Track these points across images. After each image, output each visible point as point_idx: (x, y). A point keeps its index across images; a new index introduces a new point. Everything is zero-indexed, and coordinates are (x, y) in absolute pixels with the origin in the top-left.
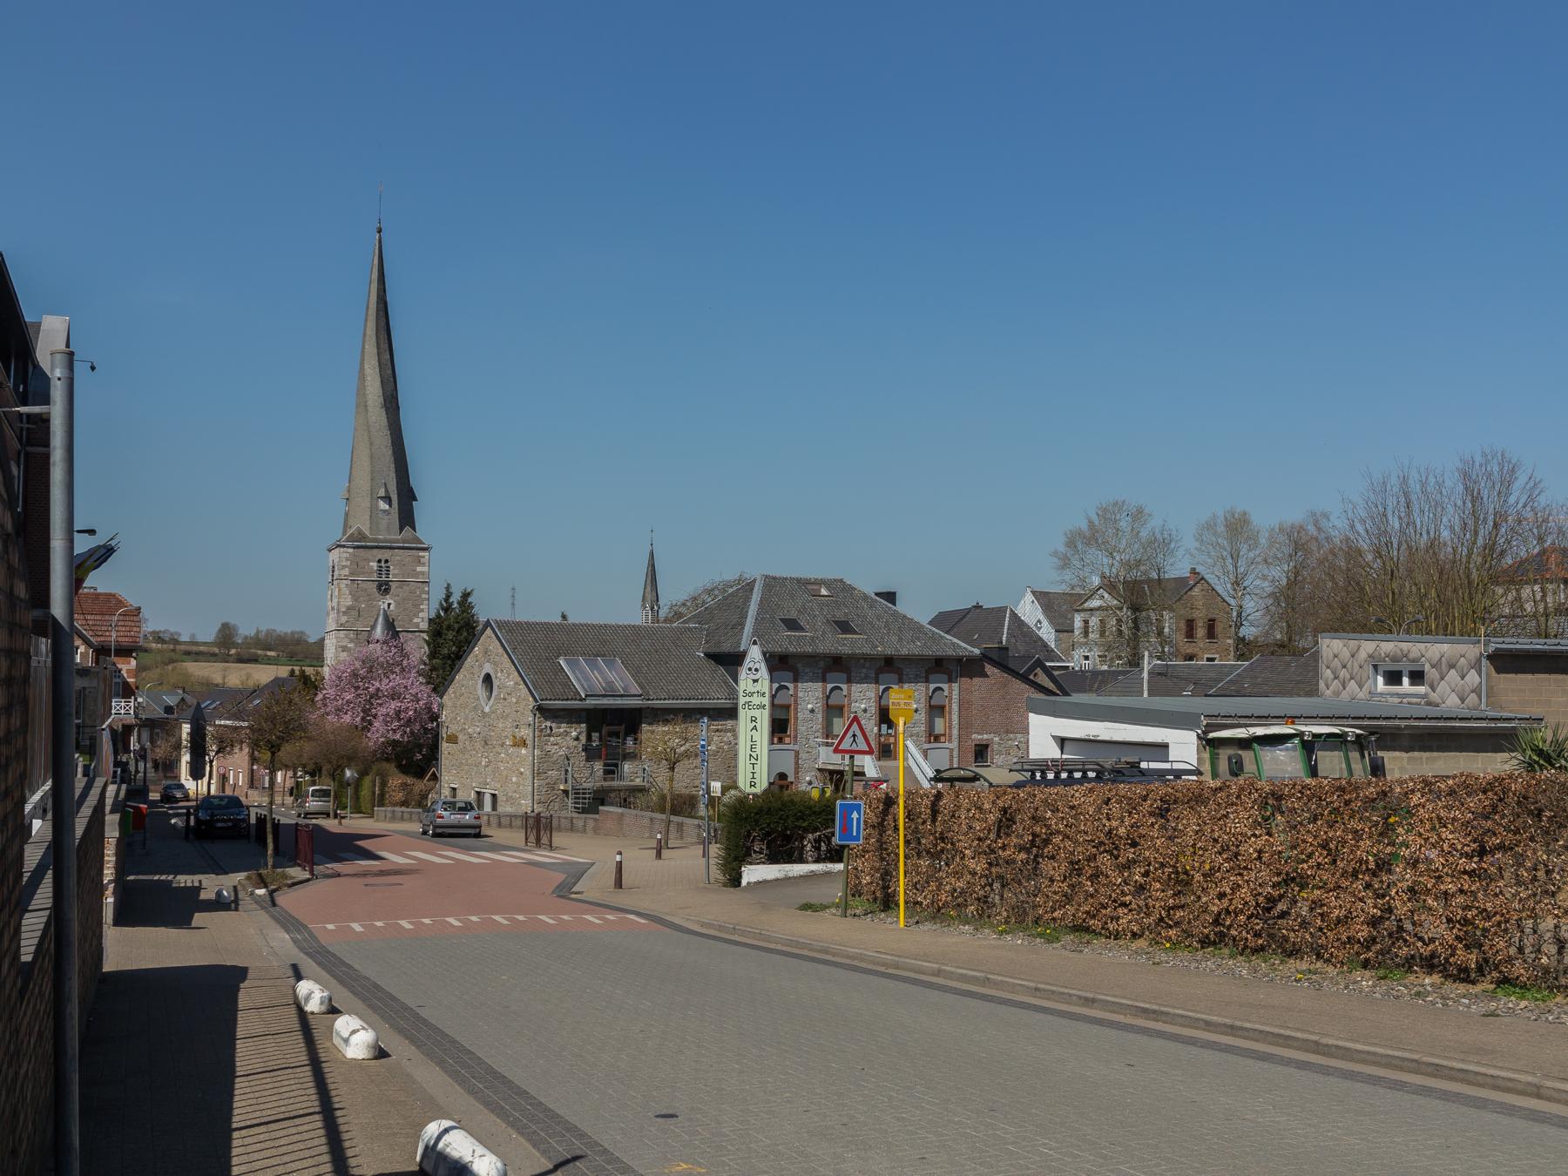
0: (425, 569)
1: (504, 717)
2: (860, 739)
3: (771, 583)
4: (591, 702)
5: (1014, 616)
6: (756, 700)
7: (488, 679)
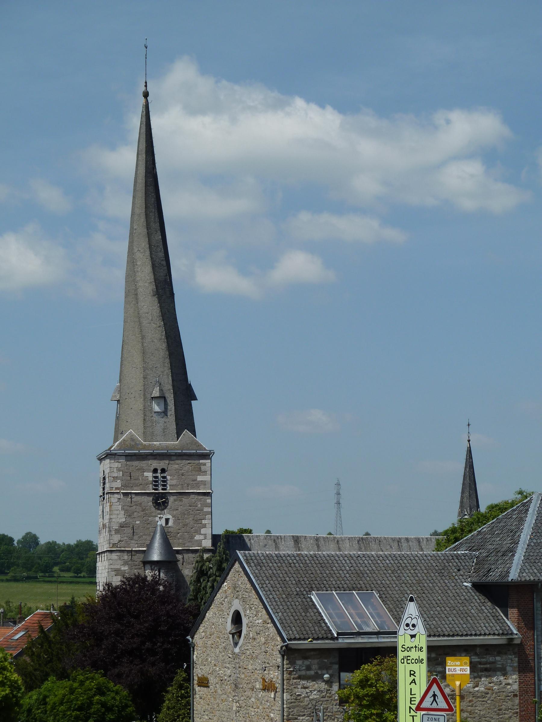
0: (207, 478)
2: (440, 699)
4: (344, 642)
6: (414, 654)
7: (237, 619)
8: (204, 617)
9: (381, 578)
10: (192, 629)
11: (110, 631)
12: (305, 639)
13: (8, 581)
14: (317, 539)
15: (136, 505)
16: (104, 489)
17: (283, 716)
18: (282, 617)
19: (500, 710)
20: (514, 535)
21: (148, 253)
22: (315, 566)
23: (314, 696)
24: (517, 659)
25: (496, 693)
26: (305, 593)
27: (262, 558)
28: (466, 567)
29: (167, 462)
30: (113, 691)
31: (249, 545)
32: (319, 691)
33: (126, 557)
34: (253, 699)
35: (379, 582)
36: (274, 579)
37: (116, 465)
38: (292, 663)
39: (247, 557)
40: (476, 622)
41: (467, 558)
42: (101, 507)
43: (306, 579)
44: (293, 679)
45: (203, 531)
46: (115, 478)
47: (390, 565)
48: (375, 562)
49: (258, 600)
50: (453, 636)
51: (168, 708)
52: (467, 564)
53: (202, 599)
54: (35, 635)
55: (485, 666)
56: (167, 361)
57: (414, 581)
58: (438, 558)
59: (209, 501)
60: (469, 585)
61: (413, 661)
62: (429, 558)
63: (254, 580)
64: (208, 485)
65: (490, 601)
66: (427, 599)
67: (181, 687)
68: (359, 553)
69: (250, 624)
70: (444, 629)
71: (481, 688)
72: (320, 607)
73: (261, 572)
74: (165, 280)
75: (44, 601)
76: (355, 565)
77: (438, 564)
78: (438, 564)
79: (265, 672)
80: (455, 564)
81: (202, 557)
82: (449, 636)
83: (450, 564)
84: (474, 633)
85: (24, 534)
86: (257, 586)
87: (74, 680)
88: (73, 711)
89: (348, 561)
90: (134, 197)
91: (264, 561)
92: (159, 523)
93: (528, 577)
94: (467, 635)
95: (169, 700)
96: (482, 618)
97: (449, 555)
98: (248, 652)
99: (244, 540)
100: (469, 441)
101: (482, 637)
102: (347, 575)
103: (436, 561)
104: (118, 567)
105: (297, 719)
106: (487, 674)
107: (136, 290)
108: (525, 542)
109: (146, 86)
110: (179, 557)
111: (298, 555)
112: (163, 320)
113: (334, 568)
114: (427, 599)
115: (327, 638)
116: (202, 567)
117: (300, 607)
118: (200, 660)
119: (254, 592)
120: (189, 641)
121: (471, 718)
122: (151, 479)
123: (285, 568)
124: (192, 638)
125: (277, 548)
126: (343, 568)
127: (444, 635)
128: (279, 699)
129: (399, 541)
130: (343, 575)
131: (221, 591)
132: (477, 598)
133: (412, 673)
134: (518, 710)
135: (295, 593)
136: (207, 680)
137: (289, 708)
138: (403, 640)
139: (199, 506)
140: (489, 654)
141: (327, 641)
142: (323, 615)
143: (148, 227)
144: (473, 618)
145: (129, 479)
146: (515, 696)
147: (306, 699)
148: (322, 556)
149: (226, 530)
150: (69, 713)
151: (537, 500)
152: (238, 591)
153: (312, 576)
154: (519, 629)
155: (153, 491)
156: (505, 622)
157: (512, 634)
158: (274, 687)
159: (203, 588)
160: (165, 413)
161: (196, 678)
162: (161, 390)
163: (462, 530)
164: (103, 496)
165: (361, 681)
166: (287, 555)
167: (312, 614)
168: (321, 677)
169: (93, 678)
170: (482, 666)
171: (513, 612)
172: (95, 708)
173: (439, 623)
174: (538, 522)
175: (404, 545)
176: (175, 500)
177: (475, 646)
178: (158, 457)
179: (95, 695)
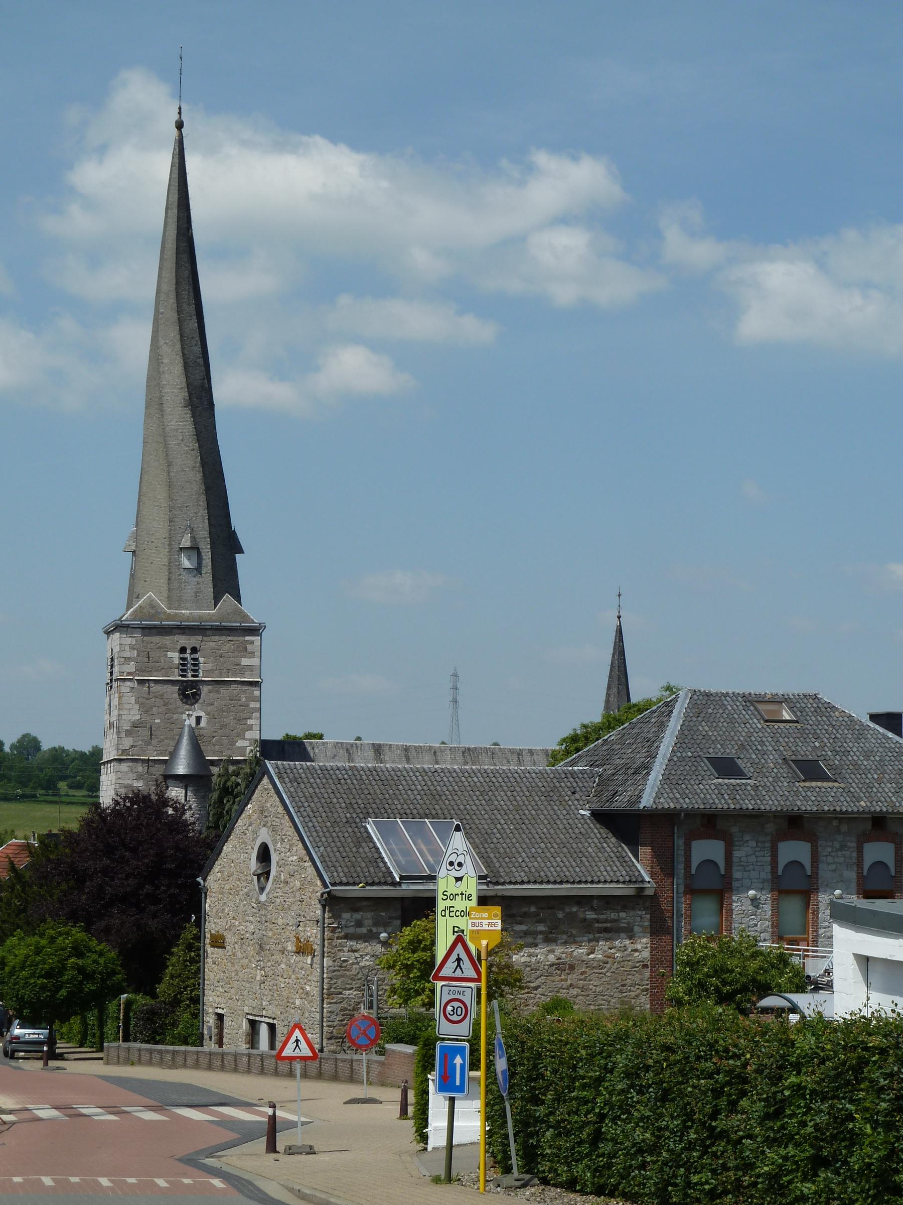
0: (255, 661)
2: (466, 964)
3: (704, 703)
6: (460, 904)
7: (264, 855)
8: (220, 852)
9: (465, 802)
11: (95, 869)
12: (354, 884)
14: (407, 749)
15: (156, 697)
16: (111, 673)
17: (323, 989)
18: (325, 854)
19: (623, 985)
20: (651, 745)
21: (178, 346)
22: (374, 783)
23: (366, 962)
24: (648, 916)
25: (619, 963)
26: (358, 820)
27: (301, 771)
28: (584, 789)
29: (200, 638)
30: (96, 952)
31: (312, 755)
32: (373, 956)
33: (140, 769)
34: (283, 966)
35: (462, 807)
36: (316, 800)
37: (129, 641)
38: (336, 916)
39: (279, 769)
40: (594, 864)
41: (585, 776)
42: (108, 698)
43: (360, 801)
44: (337, 938)
45: (248, 735)
46: (127, 660)
47: (478, 784)
48: (457, 779)
49: (293, 829)
50: (561, 882)
52: (586, 784)
53: (225, 827)
55: (605, 925)
56: (203, 497)
57: (511, 807)
58: (545, 775)
59: (257, 693)
60: (587, 813)
61: (458, 914)
62: (534, 775)
63: (287, 802)
64: (257, 672)
65: (614, 836)
66: (527, 832)
67: (190, 947)
68: (437, 766)
69: (281, 862)
70: (549, 874)
71: (598, 956)
72: (378, 839)
73: (299, 790)
74: (202, 386)
76: (429, 783)
77: (545, 784)
78: (545, 784)
79: (300, 928)
80: (568, 784)
81: (227, 770)
82: (555, 882)
83: (563, 784)
84: (590, 879)
85: (20, 736)
86: (291, 810)
87: (42, 935)
88: (38, 978)
89: (420, 778)
90: (160, 269)
91: (303, 775)
92: (187, 723)
93: (667, 804)
94: (580, 882)
95: (173, 965)
96: (603, 859)
97: (561, 772)
98: (278, 900)
99: (305, 749)
100: (619, 617)
101: (600, 886)
102: (419, 797)
103: (543, 780)
104: (129, 782)
105: (341, 993)
106: (607, 935)
107: (161, 398)
108: (665, 755)
109: (180, 113)
110: (215, 770)
111: (351, 768)
112: (198, 441)
113: (400, 787)
114: (527, 832)
115: (386, 883)
116: (226, 782)
117: (349, 840)
118: (214, 910)
119: (287, 817)
120: (199, 884)
121: (583, 995)
123: (333, 786)
124: (205, 880)
125: (350, 759)
126: (413, 787)
127: (548, 882)
128: (317, 966)
129: (520, 753)
130: (412, 797)
131: (243, 815)
132: (597, 831)
133: (456, 929)
134: (648, 987)
135: (344, 820)
136: (223, 938)
137: (331, 979)
138: (445, 884)
139: (244, 699)
140: (611, 909)
141: (385, 888)
142: (382, 851)
144: (590, 859)
145: (147, 661)
146: (645, 966)
147: (355, 966)
148: (384, 769)
149: (287, 735)
150: (32, 981)
151: (685, 698)
152: (266, 817)
153: (369, 796)
154: (652, 875)
155: (180, 678)
156: (634, 865)
157: (643, 881)
158: (312, 949)
159: (227, 812)
160: (198, 570)
161: (208, 935)
162: (193, 538)
163: (587, 738)
164: (110, 684)
165: (411, 943)
166: (335, 768)
167: (367, 849)
168: (376, 937)
169: (67, 934)
170: (600, 925)
171: (645, 852)
172: (68, 975)
173: (543, 865)
174: (684, 728)
175: (527, 758)
176: (210, 692)
178: (187, 631)
179: (69, 957)
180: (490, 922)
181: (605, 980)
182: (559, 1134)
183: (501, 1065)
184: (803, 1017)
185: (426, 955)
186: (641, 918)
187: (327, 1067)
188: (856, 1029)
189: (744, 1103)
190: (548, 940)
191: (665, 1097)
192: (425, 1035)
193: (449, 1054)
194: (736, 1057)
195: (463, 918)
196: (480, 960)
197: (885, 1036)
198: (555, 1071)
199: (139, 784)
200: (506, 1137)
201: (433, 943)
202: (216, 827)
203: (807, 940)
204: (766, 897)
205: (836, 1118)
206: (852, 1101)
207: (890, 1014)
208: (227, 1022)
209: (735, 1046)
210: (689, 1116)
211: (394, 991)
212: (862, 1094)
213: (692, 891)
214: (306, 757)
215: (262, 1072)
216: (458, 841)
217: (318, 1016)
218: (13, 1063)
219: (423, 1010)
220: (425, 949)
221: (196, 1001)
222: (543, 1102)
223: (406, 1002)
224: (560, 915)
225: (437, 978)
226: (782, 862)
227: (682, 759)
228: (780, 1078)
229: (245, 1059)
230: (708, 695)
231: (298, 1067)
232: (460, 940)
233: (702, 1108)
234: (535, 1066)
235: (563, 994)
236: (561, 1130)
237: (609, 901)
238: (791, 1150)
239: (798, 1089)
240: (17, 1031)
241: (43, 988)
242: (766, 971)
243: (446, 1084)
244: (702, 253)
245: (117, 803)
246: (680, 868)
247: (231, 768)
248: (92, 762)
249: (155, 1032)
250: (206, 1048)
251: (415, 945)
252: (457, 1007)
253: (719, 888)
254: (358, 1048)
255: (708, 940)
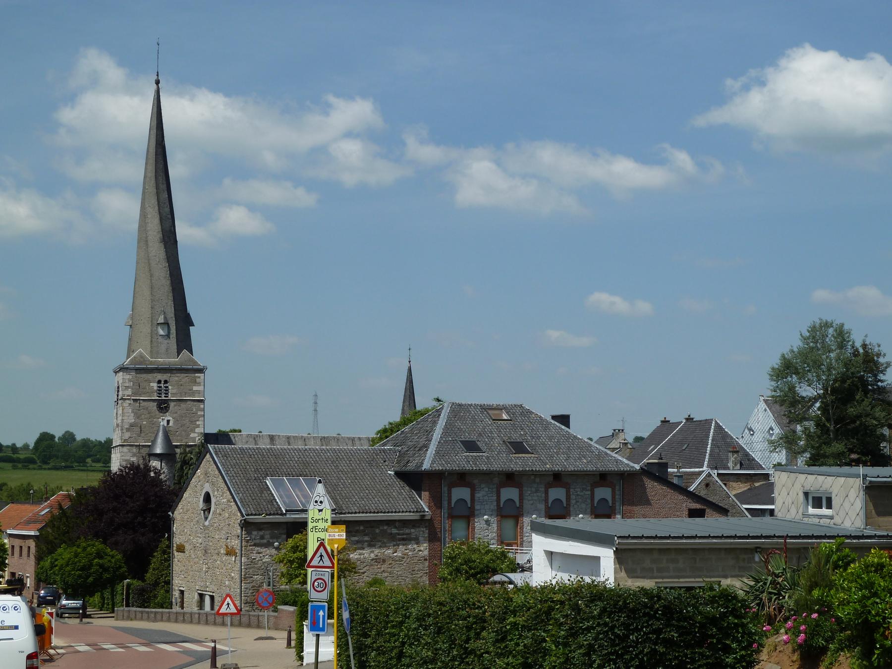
0: (201, 388)
1: (219, 529)
3: (458, 410)
5: (718, 426)
6: (321, 525)
7: (207, 499)
10: (172, 506)
12: (259, 515)
13: (49, 469)
14: (288, 438)
20: (429, 433)
21: (157, 208)
23: (267, 559)
33: (134, 450)
37: (128, 377)
45: (197, 430)
46: (127, 388)
51: (154, 569)
54: (56, 512)
56: (171, 294)
59: (202, 406)
60: (392, 473)
75: (68, 484)
87: (78, 546)
93: (438, 467)
107: (147, 237)
110: (178, 451)
112: (168, 262)
115: (277, 514)
122: (156, 388)
125: (256, 444)
129: (353, 439)
132: (398, 483)
136: (184, 547)
143: (157, 188)
145: (138, 388)
146: (426, 560)
154: (429, 507)
157: (424, 511)
160: (168, 336)
162: (165, 318)
163: (392, 430)
164: (117, 402)
165: (292, 547)
169: (93, 545)
171: (425, 494)
175: (357, 442)
177: (395, 521)
180: (339, 534)
181: (403, 567)
182: (379, 654)
183: (346, 615)
184: (516, 586)
185: (301, 555)
186: (423, 532)
187: (245, 620)
188: (547, 596)
189: (484, 634)
190: (371, 545)
191: (439, 631)
192: (301, 599)
193: (316, 610)
194: (479, 608)
195: (323, 532)
196: (333, 556)
197: (563, 594)
198: (377, 618)
199: (134, 459)
200: (349, 656)
201: (306, 547)
202: (179, 483)
203: (517, 544)
204: (494, 520)
205: (536, 641)
206: (545, 631)
207: (567, 581)
208: (186, 595)
209: (479, 602)
210: (453, 642)
211: (283, 575)
212: (550, 627)
213: (452, 517)
214: (230, 442)
215: (207, 623)
216: (320, 489)
217: (239, 591)
218: (62, 620)
219: (299, 586)
220: (300, 551)
221: (168, 583)
222: (370, 636)
223: (290, 581)
224: (377, 531)
225: (309, 566)
226: (503, 500)
227: (446, 442)
228: (505, 619)
229: (197, 616)
230: (460, 405)
231: (228, 620)
232: (322, 544)
233: (460, 638)
234: (365, 616)
235: (379, 576)
236: (380, 651)
237: (405, 523)
238: (510, 659)
239: (515, 625)
240: (64, 602)
241: (80, 576)
242: (494, 561)
243: (314, 626)
244: (428, 153)
245: (121, 470)
246: (445, 504)
247: (188, 449)
248: (106, 447)
249: (144, 601)
250: (174, 610)
251: (295, 549)
252: (319, 584)
253: (468, 515)
254: (263, 608)
255: (461, 544)
